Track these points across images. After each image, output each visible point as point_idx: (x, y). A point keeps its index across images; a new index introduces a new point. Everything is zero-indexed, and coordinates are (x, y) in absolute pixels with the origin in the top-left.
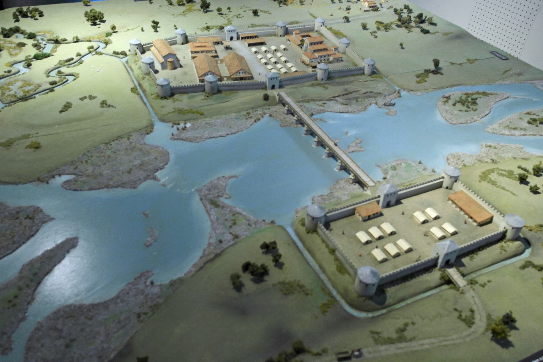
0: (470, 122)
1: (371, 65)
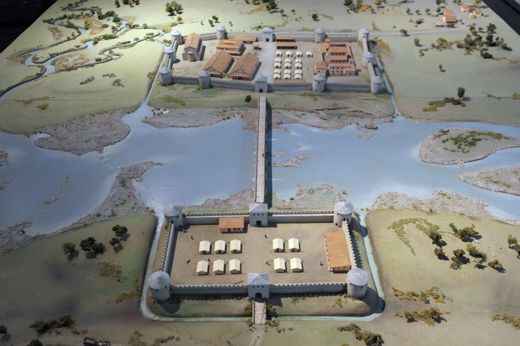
0: (447, 163)
1: (377, 84)
